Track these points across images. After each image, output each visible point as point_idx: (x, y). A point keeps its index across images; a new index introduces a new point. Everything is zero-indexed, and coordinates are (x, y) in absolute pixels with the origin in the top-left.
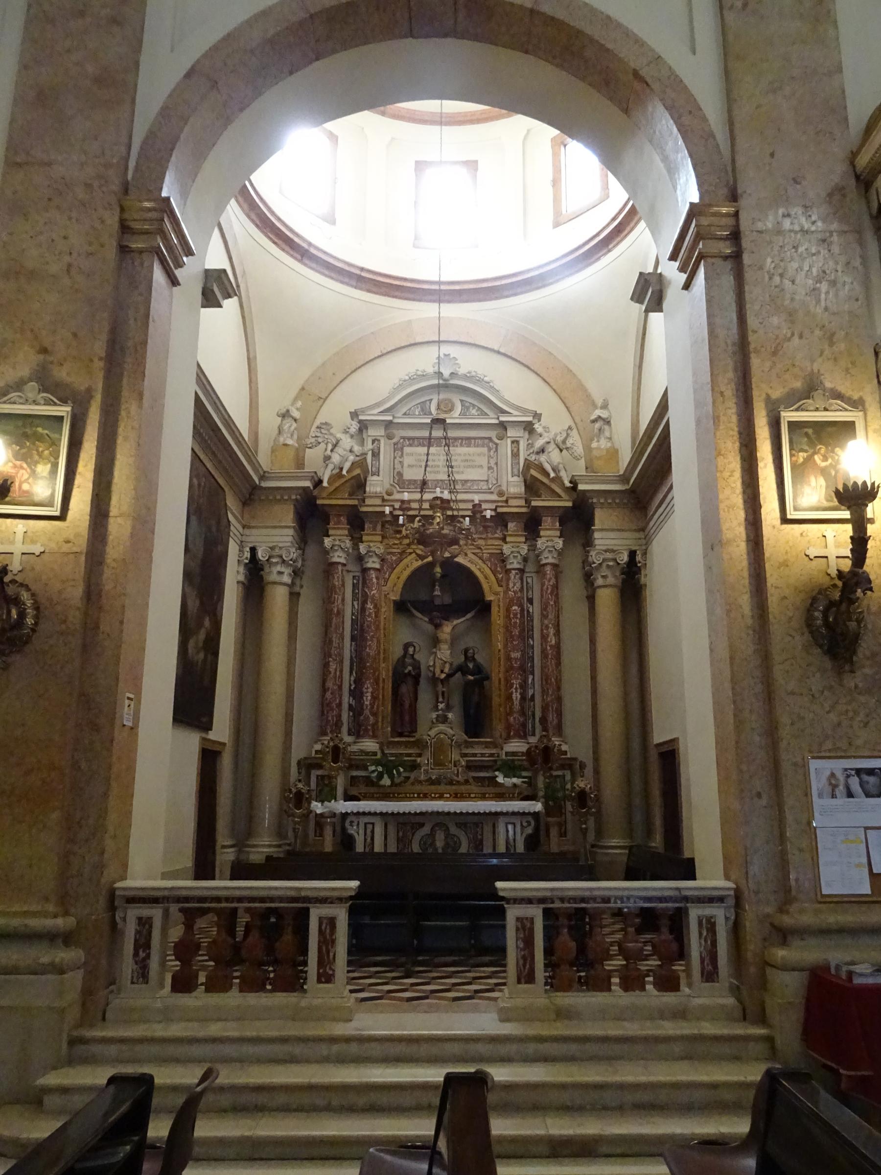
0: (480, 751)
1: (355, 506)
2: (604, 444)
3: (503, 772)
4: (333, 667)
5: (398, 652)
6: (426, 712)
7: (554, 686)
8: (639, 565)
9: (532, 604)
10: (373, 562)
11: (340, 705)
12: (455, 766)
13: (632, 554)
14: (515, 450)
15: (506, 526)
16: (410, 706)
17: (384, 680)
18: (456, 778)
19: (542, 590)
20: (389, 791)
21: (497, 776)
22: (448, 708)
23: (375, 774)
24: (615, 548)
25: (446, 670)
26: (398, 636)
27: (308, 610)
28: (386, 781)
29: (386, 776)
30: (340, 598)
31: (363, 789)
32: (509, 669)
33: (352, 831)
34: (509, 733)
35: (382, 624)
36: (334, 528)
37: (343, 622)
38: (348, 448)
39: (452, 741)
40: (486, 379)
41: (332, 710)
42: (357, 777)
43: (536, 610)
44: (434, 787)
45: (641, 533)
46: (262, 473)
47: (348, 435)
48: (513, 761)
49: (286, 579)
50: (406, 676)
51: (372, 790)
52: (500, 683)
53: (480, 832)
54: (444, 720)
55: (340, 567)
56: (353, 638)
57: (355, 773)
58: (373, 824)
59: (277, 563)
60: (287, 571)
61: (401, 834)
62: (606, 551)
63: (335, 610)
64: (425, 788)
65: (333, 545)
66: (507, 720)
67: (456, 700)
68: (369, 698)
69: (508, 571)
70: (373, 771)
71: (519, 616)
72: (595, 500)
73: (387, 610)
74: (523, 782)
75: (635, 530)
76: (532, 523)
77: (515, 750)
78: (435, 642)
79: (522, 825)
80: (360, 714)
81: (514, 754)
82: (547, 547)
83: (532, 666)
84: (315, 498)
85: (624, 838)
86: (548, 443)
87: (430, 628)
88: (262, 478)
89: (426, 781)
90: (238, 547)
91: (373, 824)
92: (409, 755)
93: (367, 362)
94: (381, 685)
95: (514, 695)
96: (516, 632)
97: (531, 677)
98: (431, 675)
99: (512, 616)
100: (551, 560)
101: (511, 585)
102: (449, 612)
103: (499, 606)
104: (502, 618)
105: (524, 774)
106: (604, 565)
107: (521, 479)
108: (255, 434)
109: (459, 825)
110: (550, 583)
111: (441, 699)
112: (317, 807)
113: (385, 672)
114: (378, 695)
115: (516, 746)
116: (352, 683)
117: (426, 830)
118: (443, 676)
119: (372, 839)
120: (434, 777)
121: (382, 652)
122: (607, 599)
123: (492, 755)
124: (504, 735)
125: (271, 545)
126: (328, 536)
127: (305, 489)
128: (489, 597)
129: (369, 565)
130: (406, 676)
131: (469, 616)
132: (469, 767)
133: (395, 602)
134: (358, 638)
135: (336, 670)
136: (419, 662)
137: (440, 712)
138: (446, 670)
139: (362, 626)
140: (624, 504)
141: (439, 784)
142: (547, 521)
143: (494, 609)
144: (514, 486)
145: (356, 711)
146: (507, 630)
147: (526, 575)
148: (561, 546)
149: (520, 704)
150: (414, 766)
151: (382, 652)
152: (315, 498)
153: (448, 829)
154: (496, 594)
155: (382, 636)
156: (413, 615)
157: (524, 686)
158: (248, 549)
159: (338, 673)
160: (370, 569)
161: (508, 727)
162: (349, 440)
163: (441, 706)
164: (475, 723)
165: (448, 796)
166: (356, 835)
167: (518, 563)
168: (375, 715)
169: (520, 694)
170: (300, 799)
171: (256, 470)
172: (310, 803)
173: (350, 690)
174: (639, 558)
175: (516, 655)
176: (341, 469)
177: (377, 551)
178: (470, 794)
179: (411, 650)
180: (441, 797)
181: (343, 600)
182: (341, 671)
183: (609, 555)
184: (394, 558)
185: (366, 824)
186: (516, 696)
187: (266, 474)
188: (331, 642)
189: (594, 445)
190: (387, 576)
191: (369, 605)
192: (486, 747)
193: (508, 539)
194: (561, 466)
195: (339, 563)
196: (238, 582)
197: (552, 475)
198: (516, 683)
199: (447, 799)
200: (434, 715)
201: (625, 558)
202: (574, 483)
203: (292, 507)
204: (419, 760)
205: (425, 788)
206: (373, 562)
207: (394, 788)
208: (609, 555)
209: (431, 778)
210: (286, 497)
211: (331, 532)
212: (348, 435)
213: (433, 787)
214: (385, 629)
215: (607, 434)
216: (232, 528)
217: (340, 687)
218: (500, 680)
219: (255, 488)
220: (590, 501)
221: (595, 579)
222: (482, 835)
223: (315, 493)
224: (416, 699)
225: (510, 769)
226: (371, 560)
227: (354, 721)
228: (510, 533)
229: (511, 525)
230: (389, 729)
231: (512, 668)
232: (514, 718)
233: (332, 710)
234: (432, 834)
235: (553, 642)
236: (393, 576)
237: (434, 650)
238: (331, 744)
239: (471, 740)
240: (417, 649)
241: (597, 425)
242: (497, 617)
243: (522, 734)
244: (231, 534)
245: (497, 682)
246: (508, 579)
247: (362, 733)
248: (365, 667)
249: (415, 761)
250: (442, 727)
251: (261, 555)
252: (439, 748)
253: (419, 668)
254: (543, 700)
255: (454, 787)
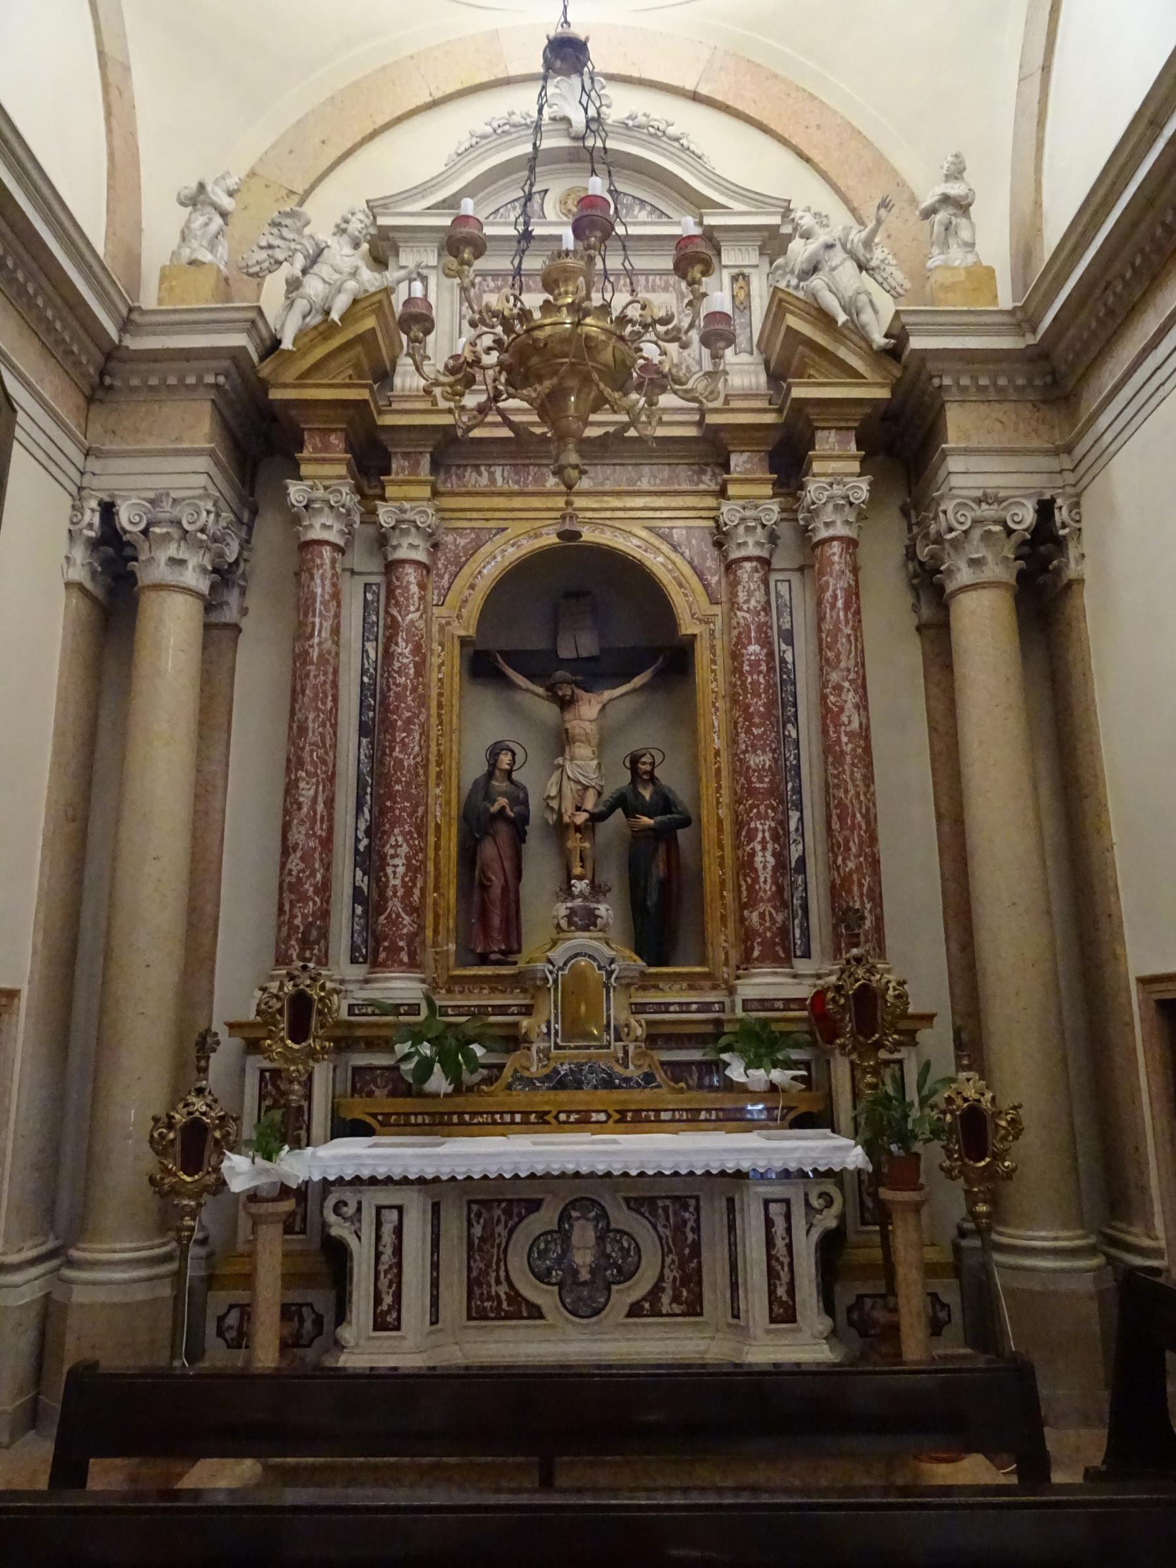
0: (679, 998)
1: (360, 405)
2: (957, 256)
3: (743, 1053)
4: (306, 791)
5: (476, 768)
6: (541, 905)
7: (854, 829)
8: (1062, 532)
9: (790, 642)
10: (411, 546)
11: (324, 888)
12: (618, 1039)
13: (1045, 509)
14: (742, 295)
15: (726, 467)
16: (505, 889)
17: (438, 827)
18: (618, 1069)
19: (819, 603)
20: (450, 1105)
21: (727, 1065)
22: (597, 891)
23: (410, 1066)
24: (1002, 494)
25: (589, 804)
26: (474, 732)
27: (257, 667)
28: (438, 1082)
29: (437, 1067)
30: (327, 625)
31: (382, 1101)
32: (744, 794)
33: (339, 1229)
34: (748, 951)
35: (434, 692)
36: (317, 460)
37: (335, 685)
38: (347, 269)
39: (610, 974)
40: (671, 131)
41: (304, 898)
42: (371, 1069)
43: (801, 657)
44: (566, 1098)
45: (1064, 457)
46: (125, 312)
47: (345, 240)
48: (765, 1023)
49: (192, 577)
50: (492, 824)
51: (404, 1104)
52: (720, 830)
53: (691, 1223)
54: (587, 920)
55: (327, 552)
56: (364, 729)
57: (362, 1059)
58: (400, 1209)
59: (167, 537)
60: (195, 559)
61: (477, 1231)
62: (979, 501)
63: (315, 654)
64: (543, 1099)
65: (310, 501)
66: (742, 920)
67: (613, 874)
68: (401, 870)
69: (730, 567)
70: (407, 1057)
71: (764, 667)
72: (947, 381)
73: (446, 664)
74: (794, 1078)
75: (1046, 452)
76: (788, 455)
77: (770, 993)
78: (562, 741)
79: (807, 1203)
80: (380, 908)
81: (765, 1004)
82: (830, 498)
83: (798, 791)
84: (264, 385)
85: (1065, 1226)
86: (829, 247)
87: (547, 711)
88: (126, 325)
89: (547, 1077)
90: (68, 501)
91: (400, 1209)
92: (502, 1010)
93: (399, 120)
94: (432, 839)
95: (759, 859)
96: (758, 705)
97: (794, 816)
98: (552, 818)
99: (746, 668)
100: (840, 530)
101: (742, 596)
102: (596, 673)
103: (713, 647)
104: (720, 677)
105: (796, 1055)
106: (977, 533)
107: (757, 357)
108: (133, 261)
109: (636, 1204)
110: (836, 584)
111: (577, 870)
112: (240, 1171)
113: (443, 809)
114: (423, 862)
115: (764, 983)
116: (361, 835)
117: (545, 1219)
118: (581, 818)
119: (398, 1251)
120: (564, 1069)
121: (433, 758)
122: (984, 621)
123: (705, 1007)
124: (735, 956)
125: (151, 495)
126: (300, 478)
127: (236, 355)
128: (688, 627)
129: (402, 553)
130: (492, 824)
131: (638, 681)
132: (653, 1039)
133: (464, 642)
134: (376, 726)
135: (314, 800)
136: (524, 789)
137: (578, 902)
138: (589, 804)
139: (384, 697)
140: (1017, 389)
141: (579, 1085)
142: (827, 441)
143: (702, 656)
144: (741, 372)
145: (370, 902)
146: (735, 701)
147: (774, 577)
148: (864, 495)
149: (775, 882)
150: (513, 1041)
151: (433, 758)
152: (264, 385)
153: (604, 1215)
154: (706, 620)
155: (434, 720)
156: (511, 685)
157: (780, 835)
158: (94, 504)
159: (320, 808)
160: (403, 562)
161: (747, 936)
162: (348, 250)
163: (580, 886)
164: (661, 924)
165: (602, 1117)
166: (352, 1241)
167: (758, 544)
168: (415, 911)
169: (774, 854)
170: (195, 1145)
171: (111, 308)
172: (221, 1157)
173: (356, 850)
174: (1061, 515)
175: (760, 759)
176: (327, 313)
177: (419, 520)
178: (658, 1111)
179: (505, 760)
180: (583, 1121)
181: (336, 631)
182: (330, 803)
183: (986, 511)
184: (462, 542)
185: (379, 1209)
186: (764, 860)
187: (135, 316)
188: (303, 730)
189: (936, 260)
190: (445, 582)
191: (403, 648)
192: (691, 988)
193: (732, 490)
194: (863, 298)
195: (327, 543)
196: (68, 585)
197: (842, 318)
198: (763, 828)
199: (601, 1128)
200: (562, 909)
201: (1027, 516)
202: (898, 335)
203: (207, 407)
204: (525, 1023)
205: (543, 1099)
206: (411, 546)
207: (460, 1100)
208: (986, 511)
209: (556, 1071)
210: (191, 380)
211: (305, 470)
212: (345, 240)
213: (563, 1096)
214: (440, 706)
215: (965, 235)
216: (21, 417)
217: (327, 843)
218: (720, 822)
219: (112, 354)
220: (936, 382)
221: (950, 572)
222: (697, 1229)
223: (265, 370)
224: (519, 876)
225: (762, 1042)
226: (405, 542)
227: (366, 927)
228: (735, 476)
229: (738, 461)
230: (452, 947)
231: (751, 791)
232: (762, 916)
233: (304, 898)
234: (562, 1234)
235: (855, 725)
236: (459, 582)
237: (560, 760)
238: (289, 987)
239: (653, 970)
240: (520, 758)
241: (941, 216)
242: (710, 674)
243: (783, 949)
244: (18, 432)
245: (713, 831)
246: (734, 584)
247: (383, 955)
248: (391, 795)
249: (516, 1025)
250: (581, 940)
251: (125, 517)
252: (575, 988)
253: (525, 803)
254: (833, 866)
255: (616, 1095)
